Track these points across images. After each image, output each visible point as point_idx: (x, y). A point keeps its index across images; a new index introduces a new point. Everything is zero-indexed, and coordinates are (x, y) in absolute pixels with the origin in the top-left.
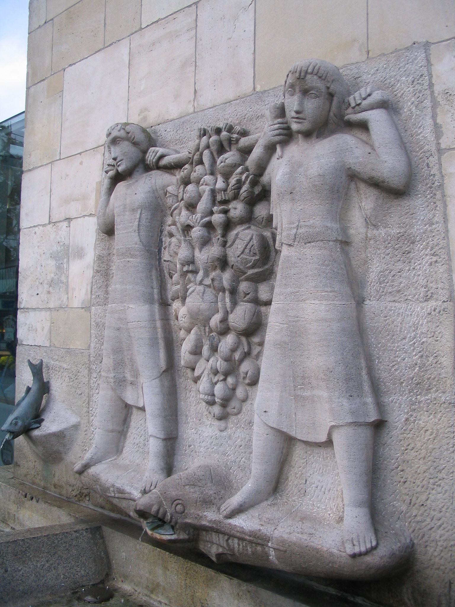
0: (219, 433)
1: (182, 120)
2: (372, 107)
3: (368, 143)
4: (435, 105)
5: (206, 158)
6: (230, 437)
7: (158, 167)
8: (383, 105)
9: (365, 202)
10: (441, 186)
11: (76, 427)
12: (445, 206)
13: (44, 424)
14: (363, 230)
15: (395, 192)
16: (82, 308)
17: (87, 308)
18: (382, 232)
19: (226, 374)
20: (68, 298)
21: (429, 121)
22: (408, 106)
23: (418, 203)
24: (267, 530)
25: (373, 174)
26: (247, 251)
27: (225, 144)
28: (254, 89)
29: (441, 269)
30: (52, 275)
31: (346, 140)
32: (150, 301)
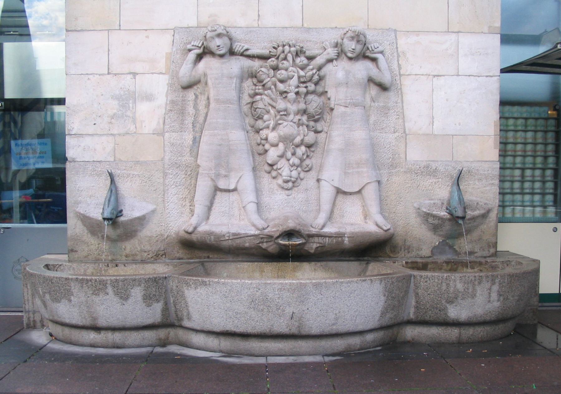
0: (287, 197)
1: (250, 29)
3: (378, 67)
4: (398, 56)
5: (290, 57)
6: (294, 198)
7: (242, 55)
8: (382, 52)
9: (374, 90)
11: (153, 211)
12: (402, 97)
13: (124, 212)
14: (369, 103)
15: (383, 88)
16: (154, 134)
17: (161, 133)
18: (376, 104)
20: (136, 127)
21: (396, 62)
22: (387, 53)
24: (342, 230)
25: (381, 81)
26: (318, 107)
27: (299, 53)
28: (303, 25)
29: (401, 121)
30: (115, 111)
32: (244, 129)
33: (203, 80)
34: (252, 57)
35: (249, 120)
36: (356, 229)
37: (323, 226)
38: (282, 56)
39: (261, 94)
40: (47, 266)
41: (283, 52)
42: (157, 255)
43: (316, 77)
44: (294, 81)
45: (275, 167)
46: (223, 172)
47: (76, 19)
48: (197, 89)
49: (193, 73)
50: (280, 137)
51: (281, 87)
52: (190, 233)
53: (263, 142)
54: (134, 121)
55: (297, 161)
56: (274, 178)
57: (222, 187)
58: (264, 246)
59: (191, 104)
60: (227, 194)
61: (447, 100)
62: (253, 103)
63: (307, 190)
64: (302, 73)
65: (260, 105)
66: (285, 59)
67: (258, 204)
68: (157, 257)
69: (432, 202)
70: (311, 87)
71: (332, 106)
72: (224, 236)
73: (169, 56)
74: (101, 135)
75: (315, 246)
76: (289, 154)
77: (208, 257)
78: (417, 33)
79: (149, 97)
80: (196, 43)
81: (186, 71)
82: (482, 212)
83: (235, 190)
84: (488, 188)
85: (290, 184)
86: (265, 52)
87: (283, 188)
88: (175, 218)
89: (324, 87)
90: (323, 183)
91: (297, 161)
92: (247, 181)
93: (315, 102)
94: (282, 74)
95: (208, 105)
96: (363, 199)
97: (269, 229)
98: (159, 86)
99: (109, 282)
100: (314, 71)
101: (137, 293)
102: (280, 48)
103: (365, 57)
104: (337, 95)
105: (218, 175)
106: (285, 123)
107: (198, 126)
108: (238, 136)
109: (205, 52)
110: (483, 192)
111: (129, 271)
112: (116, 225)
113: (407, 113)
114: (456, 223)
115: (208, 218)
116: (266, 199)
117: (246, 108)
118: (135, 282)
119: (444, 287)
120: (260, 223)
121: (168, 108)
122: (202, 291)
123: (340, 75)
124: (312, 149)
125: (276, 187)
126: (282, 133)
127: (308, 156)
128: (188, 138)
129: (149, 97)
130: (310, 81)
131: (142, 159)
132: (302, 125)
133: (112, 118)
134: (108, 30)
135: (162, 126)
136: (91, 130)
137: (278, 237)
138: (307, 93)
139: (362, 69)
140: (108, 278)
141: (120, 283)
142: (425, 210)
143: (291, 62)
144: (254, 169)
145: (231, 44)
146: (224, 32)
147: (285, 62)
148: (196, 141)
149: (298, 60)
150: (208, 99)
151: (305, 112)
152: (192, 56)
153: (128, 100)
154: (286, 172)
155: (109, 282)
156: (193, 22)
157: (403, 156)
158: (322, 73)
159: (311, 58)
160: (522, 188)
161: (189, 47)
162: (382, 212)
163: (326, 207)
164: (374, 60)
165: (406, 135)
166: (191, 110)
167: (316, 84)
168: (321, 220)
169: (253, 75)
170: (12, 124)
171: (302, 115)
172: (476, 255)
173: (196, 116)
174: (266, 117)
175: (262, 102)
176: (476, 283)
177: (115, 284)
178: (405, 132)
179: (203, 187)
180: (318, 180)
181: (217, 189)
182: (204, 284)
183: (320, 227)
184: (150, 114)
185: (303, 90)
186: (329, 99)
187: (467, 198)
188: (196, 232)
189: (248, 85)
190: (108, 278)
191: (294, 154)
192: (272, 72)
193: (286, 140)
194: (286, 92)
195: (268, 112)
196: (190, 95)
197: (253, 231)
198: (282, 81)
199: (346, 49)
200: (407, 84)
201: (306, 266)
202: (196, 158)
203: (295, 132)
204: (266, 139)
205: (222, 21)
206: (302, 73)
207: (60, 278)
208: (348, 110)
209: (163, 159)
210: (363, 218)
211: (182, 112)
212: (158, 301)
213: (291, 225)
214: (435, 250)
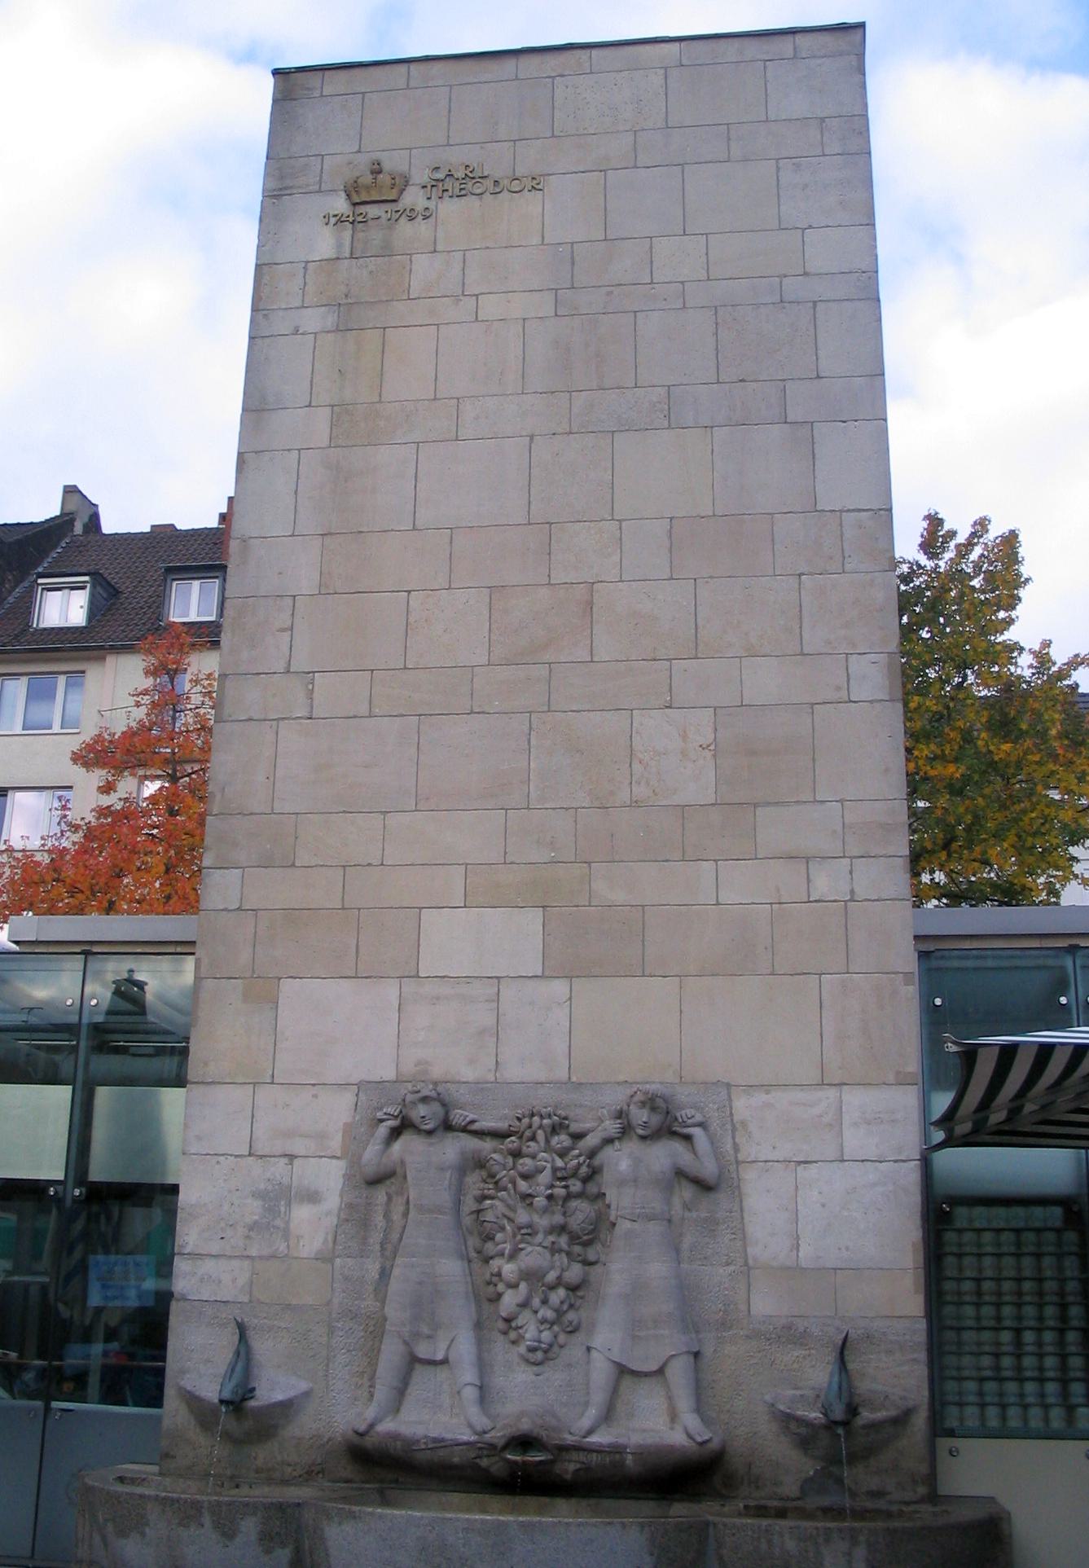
2: (694, 1125)
3: (695, 1152)
5: (540, 1135)
7: (464, 1130)
8: (700, 1125)
9: (687, 1192)
10: (739, 1187)
11: (307, 1394)
15: (704, 1186)
17: (325, 1258)
18: (694, 1214)
19: (552, 1324)
22: (714, 1125)
23: (721, 1197)
24: (621, 1441)
29: (739, 1243)
31: (677, 1146)
32: (461, 1257)
33: (398, 1170)
34: (480, 1134)
35: (473, 1242)
36: (650, 1439)
37: (590, 1432)
38: (528, 1133)
39: (492, 1198)
40: (121, 1479)
41: (530, 1127)
42: (309, 1473)
43: (584, 1170)
44: (545, 1178)
45: (514, 1324)
46: (425, 1330)
47: (206, 1064)
48: (391, 1186)
49: (384, 1160)
50: (521, 1271)
51: (523, 1185)
52: (361, 1435)
53: (495, 1279)
54: (286, 1234)
55: (550, 1314)
56: (513, 1342)
57: (421, 1356)
58: (484, 1462)
59: (380, 1210)
60: (431, 1368)
61: (823, 1206)
62: (479, 1212)
63: (570, 1365)
64: (559, 1163)
65: (489, 1216)
66: (533, 1138)
67: (483, 1390)
68: (310, 1474)
69: (798, 1393)
70: (576, 1186)
71: (612, 1218)
72: (418, 1441)
73: (348, 1129)
74: (230, 1257)
75: (572, 1467)
76: (536, 1302)
77: (397, 1481)
78: (766, 1087)
79: (313, 1197)
80: (390, 1110)
81: (371, 1153)
82: (893, 1413)
83: (445, 1362)
84: (906, 1368)
85: (539, 1355)
86: (502, 1125)
87: (527, 1361)
88: (342, 1408)
89: (599, 1186)
90: (594, 1354)
91: (550, 1314)
92: (464, 1347)
93: (581, 1212)
94: (526, 1164)
95: (406, 1214)
96: (667, 1386)
97: (492, 1434)
98: (329, 1177)
99: (206, 1505)
100: (582, 1159)
101: (250, 1527)
102: (526, 1121)
103: (674, 1134)
104: (620, 1200)
105: (417, 1335)
106: (530, 1249)
107: (389, 1247)
108: (451, 1268)
109: (403, 1126)
110: (897, 1377)
111: (245, 1494)
112: (241, 1415)
113: (750, 1229)
114: (842, 1434)
115: (398, 1410)
116: (498, 1380)
117: (467, 1221)
118: (249, 1508)
119: (764, 1546)
120: (481, 1421)
121: (343, 1216)
122: (348, 1528)
123: (624, 1165)
124: (580, 1294)
125: (516, 1359)
126: (523, 1266)
127: (571, 1306)
128: (373, 1268)
129: (313, 1197)
130: (574, 1175)
131: (294, 1302)
132: (560, 1251)
133: (251, 1229)
134: (254, 1084)
135: (331, 1245)
136: (215, 1247)
137: (505, 1447)
138: (569, 1197)
139: (662, 1155)
140: (205, 1498)
141: (224, 1508)
142: (782, 1407)
143: (542, 1144)
144: (478, 1326)
145: (447, 1113)
146: (433, 1094)
147: (532, 1144)
148: (385, 1274)
149: (555, 1140)
150: (408, 1202)
151: (562, 1229)
152: (383, 1130)
153: (278, 1199)
154: (530, 1332)
155: (206, 1505)
156: (389, 1074)
157: (743, 1307)
158: (596, 1162)
159: (577, 1137)
160: (1019, 1368)
161: (380, 1115)
162: (699, 1409)
163: (598, 1398)
164: (688, 1138)
165: (749, 1269)
166: (379, 1220)
167: (586, 1180)
168: (586, 1422)
169: (480, 1163)
170: (103, 1217)
171: (559, 1235)
172: (888, 1497)
173: (387, 1231)
174: (499, 1236)
175: (495, 1209)
176: (821, 1540)
177: (215, 1509)
178: (746, 1264)
179: (391, 1354)
180: (589, 1349)
181: (413, 1361)
182: (353, 1516)
183: (583, 1433)
184: (312, 1226)
185: (560, 1192)
186: (609, 1206)
187: (863, 1387)
188: (372, 1433)
189: (474, 1181)
190: (205, 1498)
191: (545, 1302)
192: (510, 1160)
193: (531, 1276)
194: (530, 1195)
195: (503, 1229)
196: (380, 1195)
197: (467, 1436)
198: (525, 1177)
199: (634, 1122)
200: (750, 1177)
201: (561, 1504)
202: (383, 1302)
203: (545, 1264)
204: (499, 1274)
205: (437, 1072)
206: (559, 1163)
207: (131, 1495)
208: (636, 1226)
209: (329, 1303)
210: (668, 1420)
211: (365, 1224)
212: (283, 1545)
213: (525, 1426)
214: (808, 1486)
